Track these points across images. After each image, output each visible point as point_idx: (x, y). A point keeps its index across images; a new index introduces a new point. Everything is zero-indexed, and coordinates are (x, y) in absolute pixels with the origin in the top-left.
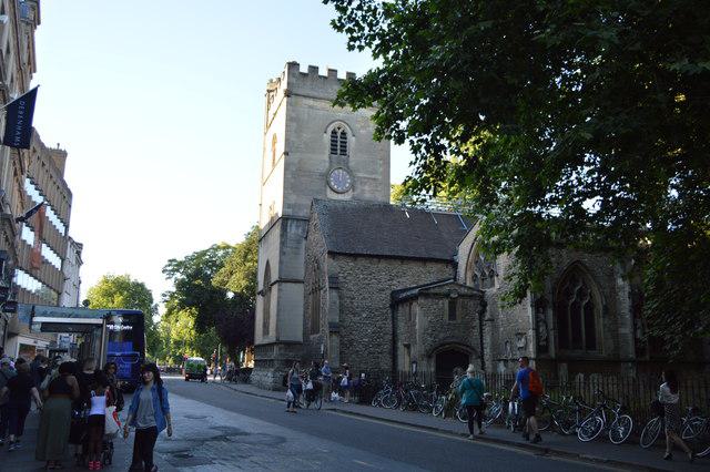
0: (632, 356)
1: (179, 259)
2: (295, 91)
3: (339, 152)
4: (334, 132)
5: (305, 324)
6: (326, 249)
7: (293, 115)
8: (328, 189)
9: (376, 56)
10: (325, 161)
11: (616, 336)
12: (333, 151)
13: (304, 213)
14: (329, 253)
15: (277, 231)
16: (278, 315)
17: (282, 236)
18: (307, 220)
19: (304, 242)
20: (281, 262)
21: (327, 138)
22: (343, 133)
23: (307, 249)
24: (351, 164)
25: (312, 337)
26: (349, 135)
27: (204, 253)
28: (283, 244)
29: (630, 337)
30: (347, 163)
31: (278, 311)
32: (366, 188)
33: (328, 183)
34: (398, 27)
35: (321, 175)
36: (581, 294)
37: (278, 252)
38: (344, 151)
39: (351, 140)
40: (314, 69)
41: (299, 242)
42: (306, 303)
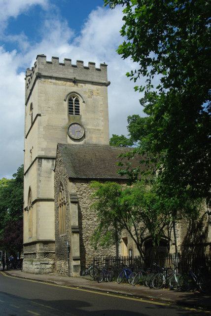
4: (70, 100)
10: (65, 119)
12: (70, 111)
21: (66, 104)
22: (77, 101)
24: (83, 120)
26: (81, 102)
32: (94, 136)
33: (68, 133)
35: (64, 128)
39: (82, 106)
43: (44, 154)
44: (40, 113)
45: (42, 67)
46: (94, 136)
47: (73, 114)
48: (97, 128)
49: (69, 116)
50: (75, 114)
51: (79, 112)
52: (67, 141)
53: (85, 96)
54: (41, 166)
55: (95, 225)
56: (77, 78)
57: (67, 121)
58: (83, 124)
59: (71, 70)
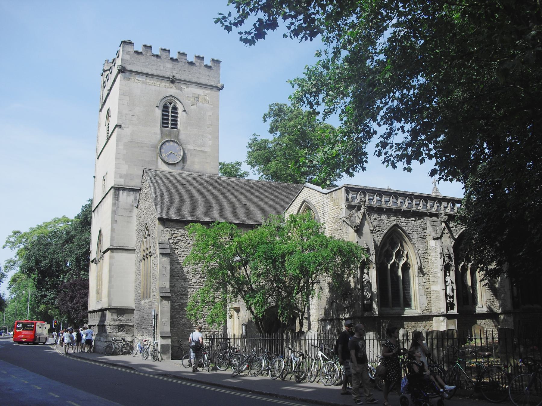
0: (443, 310)
1: (23, 232)
2: (129, 67)
3: (170, 126)
4: (165, 107)
5: (136, 289)
6: (155, 216)
7: (348, 370)
8: (160, 160)
9: (271, 131)
10: (156, 134)
11: (428, 292)
12: (164, 124)
13: (135, 183)
14: (161, 220)
15: (110, 199)
16: (110, 282)
17: (114, 204)
18: (138, 190)
19: (136, 211)
20: (113, 230)
21: (158, 113)
22: (175, 108)
23: (139, 218)
24: (182, 137)
25: (143, 302)
27: (47, 225)
28: (114, 212)
29: (442, 293)
30: (177, 136)
31: (110, 277)
32: (196, 160)
34: (473, 387)
35: (155, 147)
36: (399, 255)
37: (110, 220)
38: (175, 124)
40: (148, 47)
41: (131, 211)
42: (139, 269)
43: (123, 183)
44: (120, 123)
45: (128, 57)
46: (196, 160)
47: (168, 127)
48: (203, 149)
49: (161, 130)
50: (172, 128)
51: (176, 125)
52: (157, 166)
53: (187, 102)
54: (117, 200)
55: (194, 288)
56: (178, 76)
57: (159, 136)
58: (182, 141)
59: (169, 65)
